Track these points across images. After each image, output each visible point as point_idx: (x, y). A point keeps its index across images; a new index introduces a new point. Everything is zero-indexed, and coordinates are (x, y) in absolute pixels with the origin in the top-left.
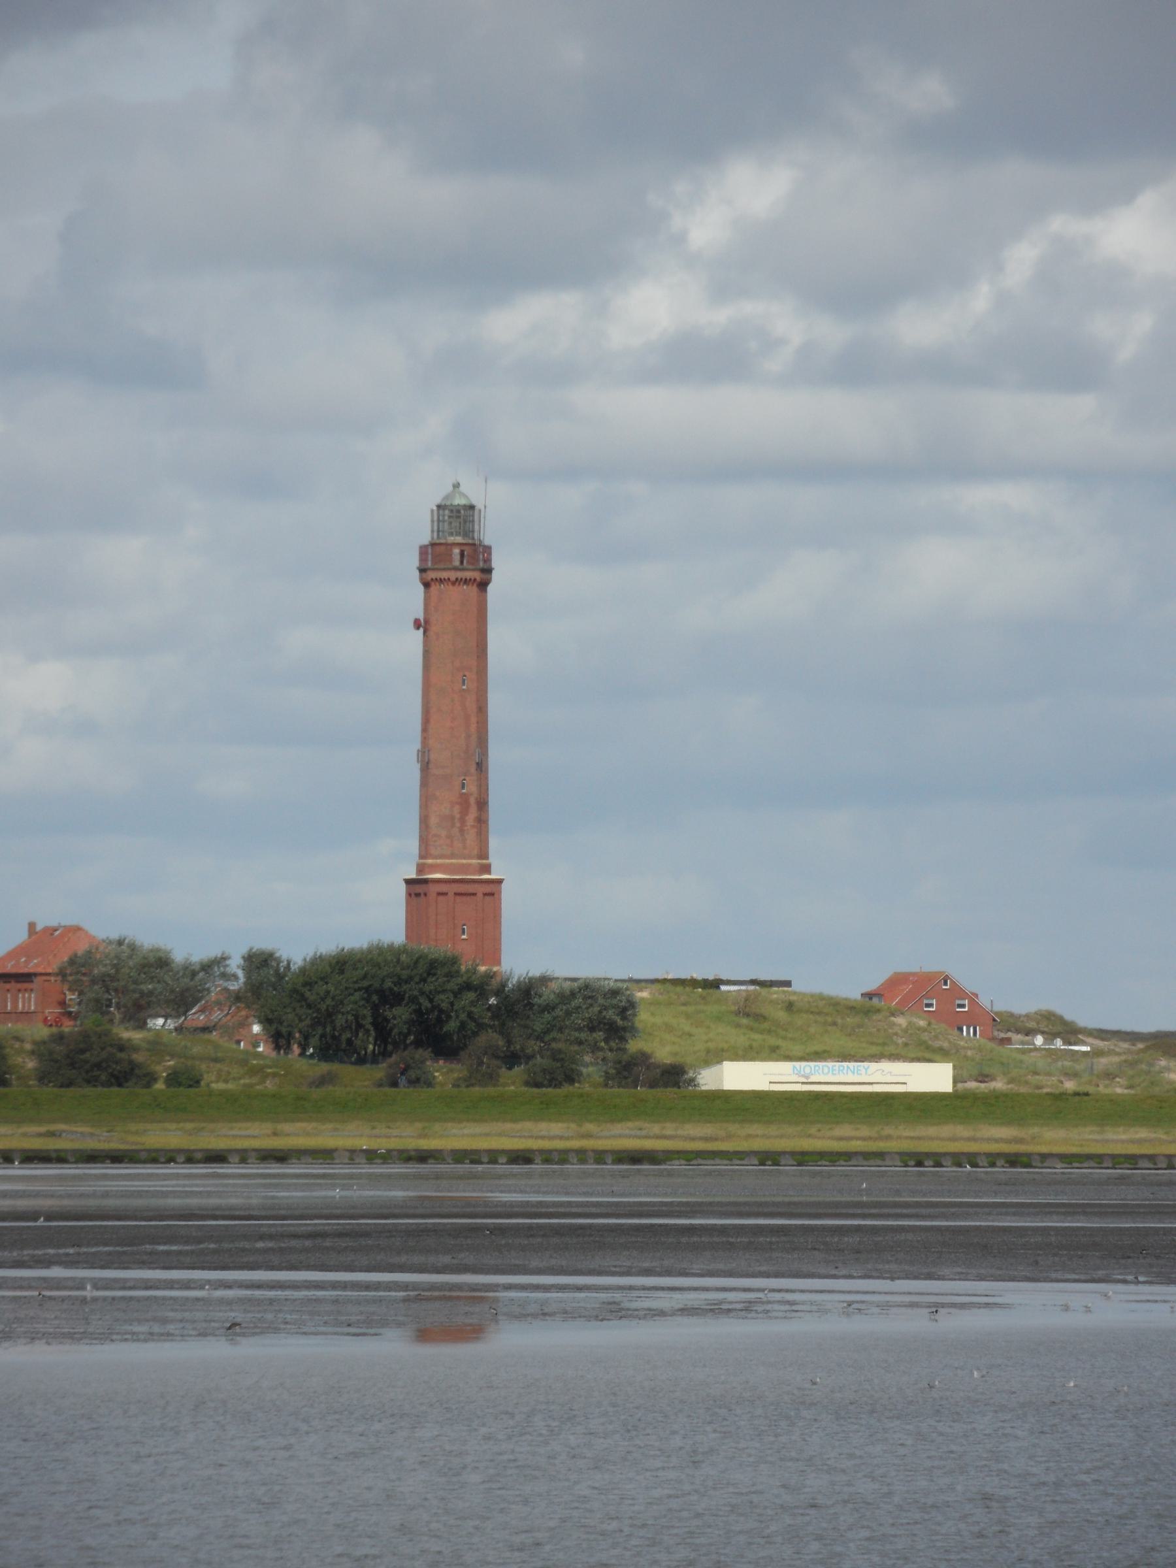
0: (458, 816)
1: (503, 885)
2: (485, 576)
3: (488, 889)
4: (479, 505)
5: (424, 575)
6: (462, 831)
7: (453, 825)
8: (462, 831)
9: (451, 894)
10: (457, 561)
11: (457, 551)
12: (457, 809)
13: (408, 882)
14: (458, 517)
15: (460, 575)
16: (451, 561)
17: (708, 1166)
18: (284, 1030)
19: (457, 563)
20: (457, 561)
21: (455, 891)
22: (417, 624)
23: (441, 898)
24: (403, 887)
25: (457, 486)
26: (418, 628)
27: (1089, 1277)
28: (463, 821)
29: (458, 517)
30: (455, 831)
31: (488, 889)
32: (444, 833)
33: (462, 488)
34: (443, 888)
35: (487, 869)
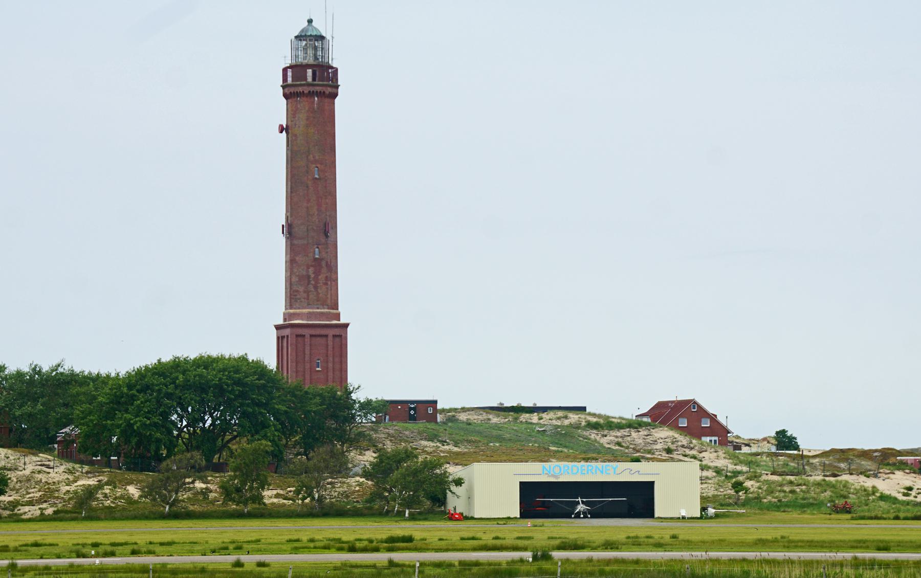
0: (313, 276)
1: (349, 329)
2: (334, 90)
3: (337, 331)
4: (328, 37)
5: (286, 90)
6: (316, 287)
7: (309, 283)
8: (316, 287)
9: (308, 336)
10: (311, 86)
11: (309, 72)
12: (311, 270)
13: (278, 328)
14: (311, 39)
15: (312, 89)
16: (306, 79)
17: (873, 515)
18: (322, 465)
19: (310, 79)
20: (311, 86)
21: (315, 334)
22: (281, 129)
23: (299, 339)
24: (274, 333)
25: (310, 21)
26: (281, 132)
27: (524, 417)
28: (316, 279)
29: (311, 39)
30: (311, 288)
31: (337, 331)
32: (301, 289)
33: (313, 24)
34: (300, 331)
35: (338, 317)
